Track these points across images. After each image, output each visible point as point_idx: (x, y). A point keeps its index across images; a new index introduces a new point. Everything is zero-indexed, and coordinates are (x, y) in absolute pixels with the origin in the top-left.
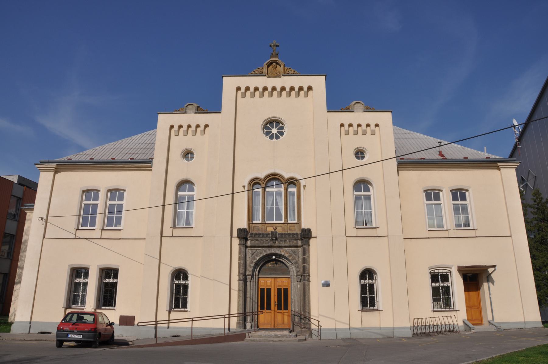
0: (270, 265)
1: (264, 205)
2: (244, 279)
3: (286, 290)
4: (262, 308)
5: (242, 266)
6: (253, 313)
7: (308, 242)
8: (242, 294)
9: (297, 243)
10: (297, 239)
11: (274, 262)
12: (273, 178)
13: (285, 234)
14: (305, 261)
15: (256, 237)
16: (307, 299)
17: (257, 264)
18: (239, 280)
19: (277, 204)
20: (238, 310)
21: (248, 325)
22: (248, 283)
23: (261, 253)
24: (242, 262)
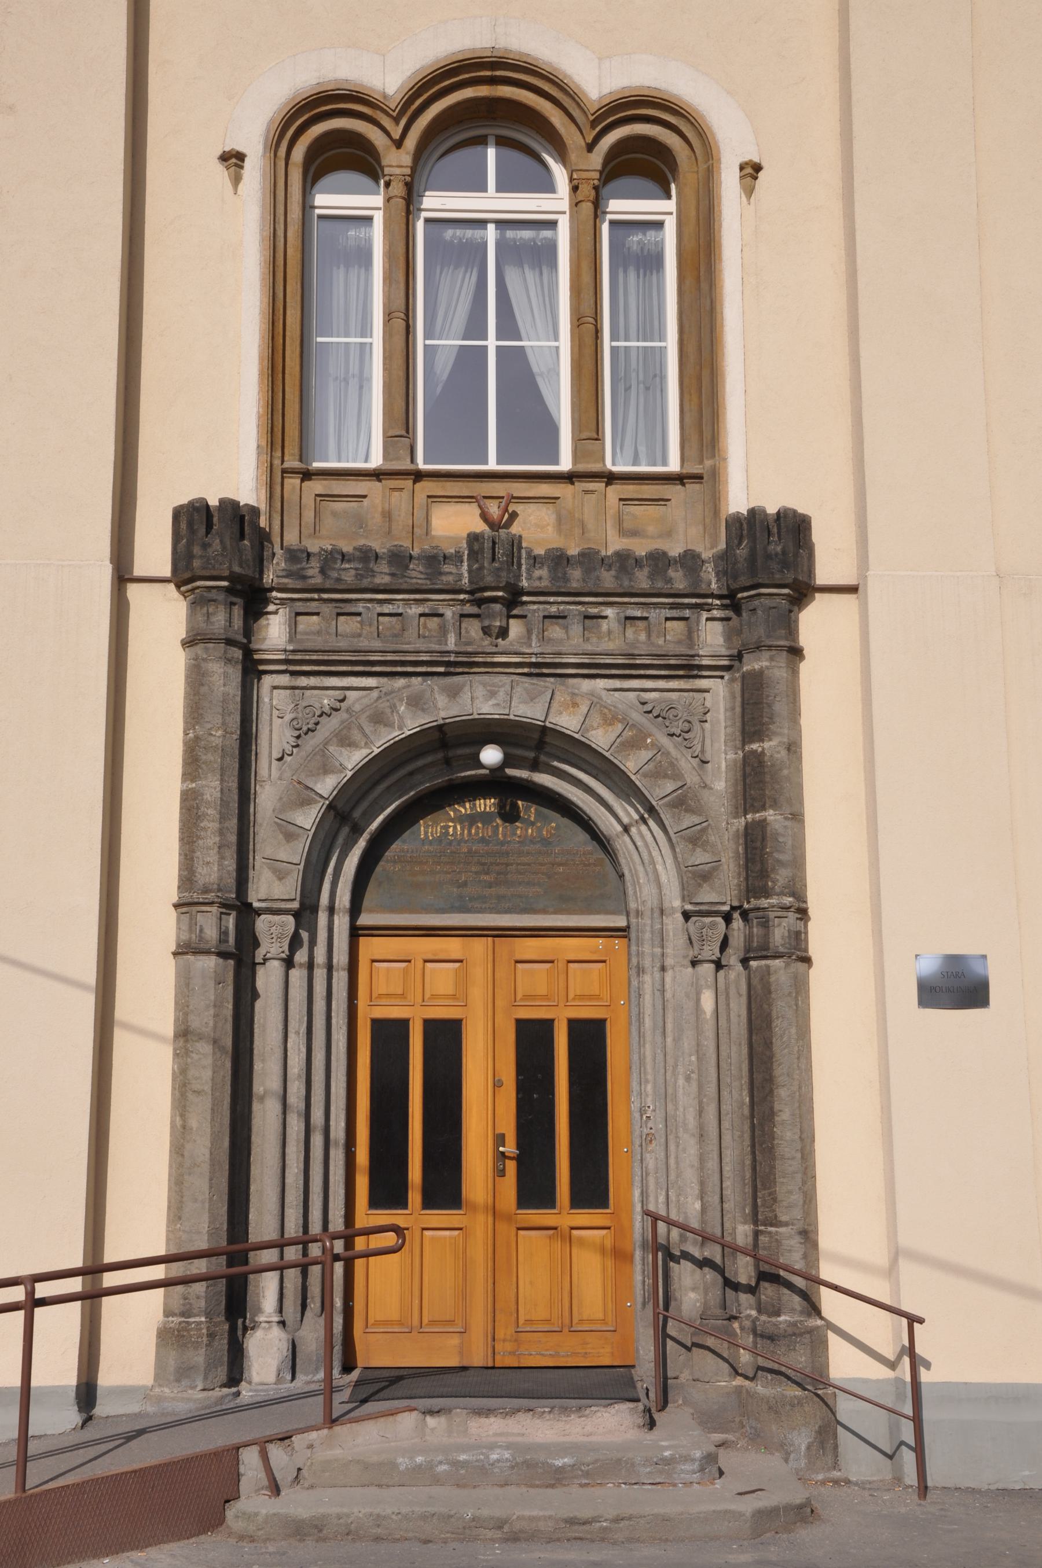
0: (455, 829)
1: (409, 330)
2: (230, 936)
3: (589, 1038)
4: (388, 1191)
5: (210, 825)
6: (304, 1242)
7: (791, 629)
8: (210, 1068)
9: (690, 635)
10: (688, 602)
11: (486, 805)
12: (488, 106)
13: (589, 559)
14: (764, 781)
15: (339, 579)
16: (785, 1114)
17: (341, 816)
18: (184, 950)
19: (508, 327)
20: (176, 1212)
21: (265, 1351)
22: (268, 978)
23: (379, 719)
24: (211, 788)
